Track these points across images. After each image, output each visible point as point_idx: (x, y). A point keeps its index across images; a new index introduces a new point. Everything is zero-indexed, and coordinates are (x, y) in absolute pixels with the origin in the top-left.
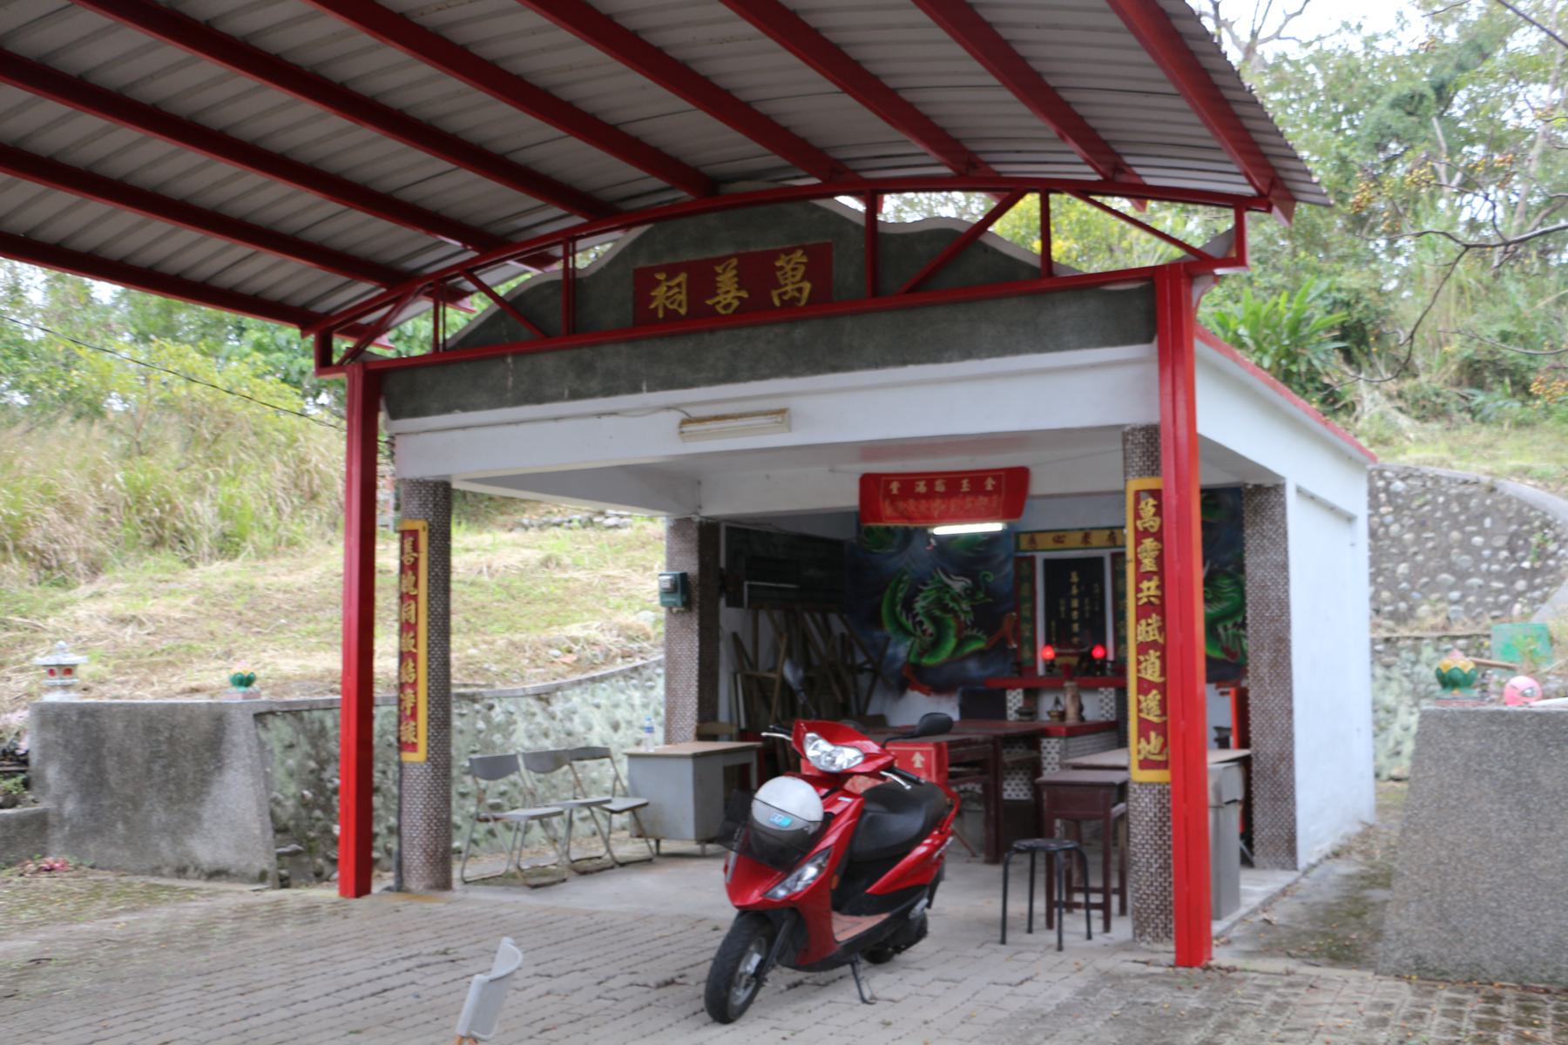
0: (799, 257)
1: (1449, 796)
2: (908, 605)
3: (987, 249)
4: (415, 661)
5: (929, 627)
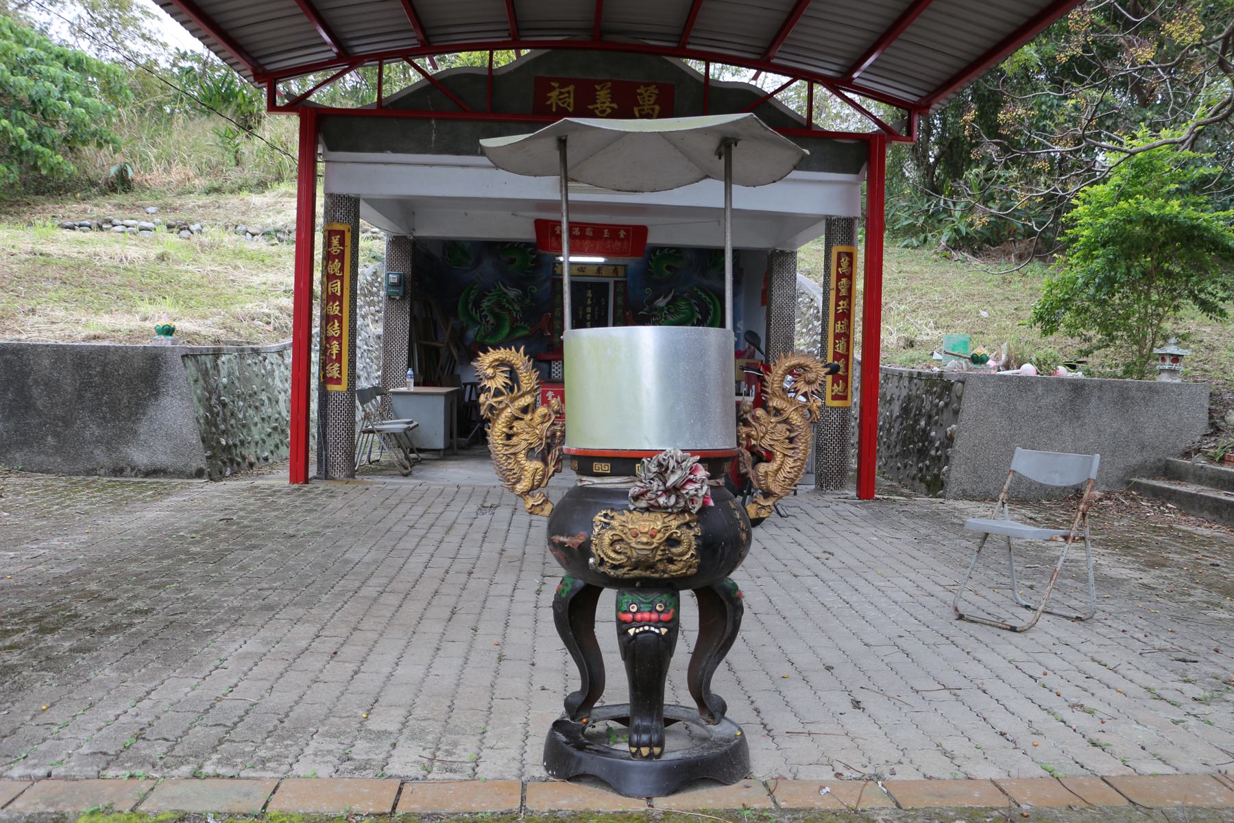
0: (653, 89)
2: (477, 304)
3: (770, 106)
4: (341, 322)
5: (490, 319)
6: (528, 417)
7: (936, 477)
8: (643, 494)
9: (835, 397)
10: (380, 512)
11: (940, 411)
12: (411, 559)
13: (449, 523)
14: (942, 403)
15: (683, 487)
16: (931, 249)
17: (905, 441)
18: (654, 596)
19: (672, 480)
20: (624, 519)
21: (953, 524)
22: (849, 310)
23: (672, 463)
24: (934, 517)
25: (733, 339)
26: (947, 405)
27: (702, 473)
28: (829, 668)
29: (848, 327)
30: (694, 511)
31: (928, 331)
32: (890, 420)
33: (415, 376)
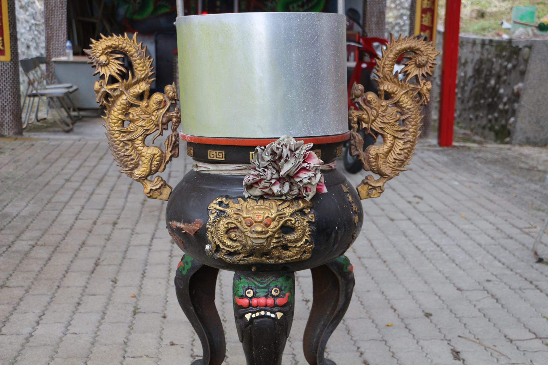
6: (144, 104)
7: (504, 127)
8: (257, 183)
10: (42, 166)
11: (508, 72)
12: (65, 212)
13: (100, 176)
14: (510, 66)
15: (296, 175)
17: (477, 97)
18: (270, 280)
19: (286, 168)
20: (238, 207)
21: (521, 168)
23: (286, 152)
24: (505, 162)
25: (344, 23)
26: (514, 67)
27: (315, 161)
28: (428, 315)
30: (308, 199)
32: (465, 80)
33: (73, 47)
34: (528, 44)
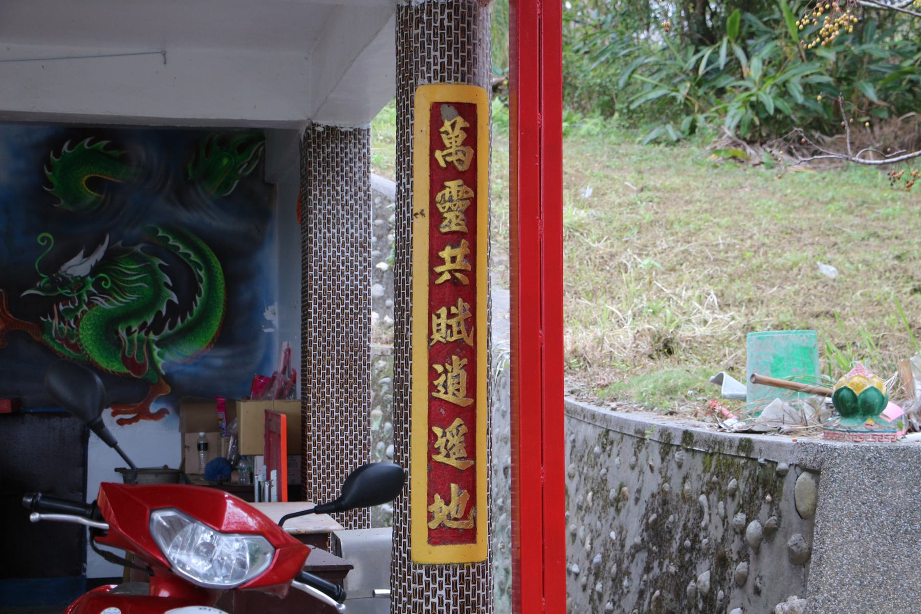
1: (874, 568)
9: (438, 536)
14: (754, 528)
16: (703, 144)
22: (472, 275)
26: (769, 533)
29: (471, 323)
31: (706, 313)
34: (808, 460)
